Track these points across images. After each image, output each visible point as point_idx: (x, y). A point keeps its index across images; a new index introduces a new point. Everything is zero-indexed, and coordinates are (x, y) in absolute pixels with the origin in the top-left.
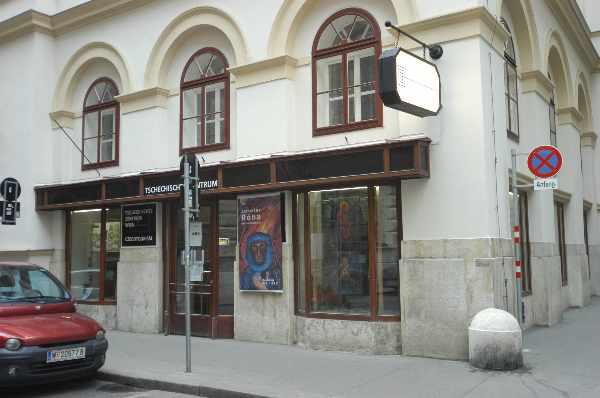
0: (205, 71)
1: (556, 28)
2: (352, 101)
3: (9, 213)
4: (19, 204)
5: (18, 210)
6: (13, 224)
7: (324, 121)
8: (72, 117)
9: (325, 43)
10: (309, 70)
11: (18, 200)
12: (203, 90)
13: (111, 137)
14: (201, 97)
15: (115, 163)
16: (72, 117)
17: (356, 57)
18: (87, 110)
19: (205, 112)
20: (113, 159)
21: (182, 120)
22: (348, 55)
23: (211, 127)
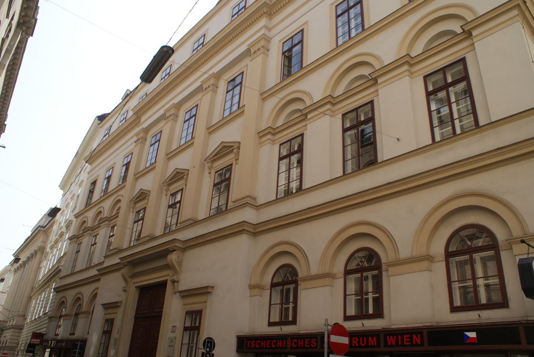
0: (284, 277)
1: (475, 265)
2: (367, 300)
7: (275, 318)
8: (429, 258)
9: (353, 266)
10: (269, 291)
11: (213, 352)
12: (283, 288)
13: (284, 307)
14: (282, 291)
15: (294, 322)
16: (429, 258)
17: (370, 274)
18: (273, 285)
19: (285, 300)
20: (197, 325)
21: (270, 305)
22: (364, 273)
23: (287, 309)
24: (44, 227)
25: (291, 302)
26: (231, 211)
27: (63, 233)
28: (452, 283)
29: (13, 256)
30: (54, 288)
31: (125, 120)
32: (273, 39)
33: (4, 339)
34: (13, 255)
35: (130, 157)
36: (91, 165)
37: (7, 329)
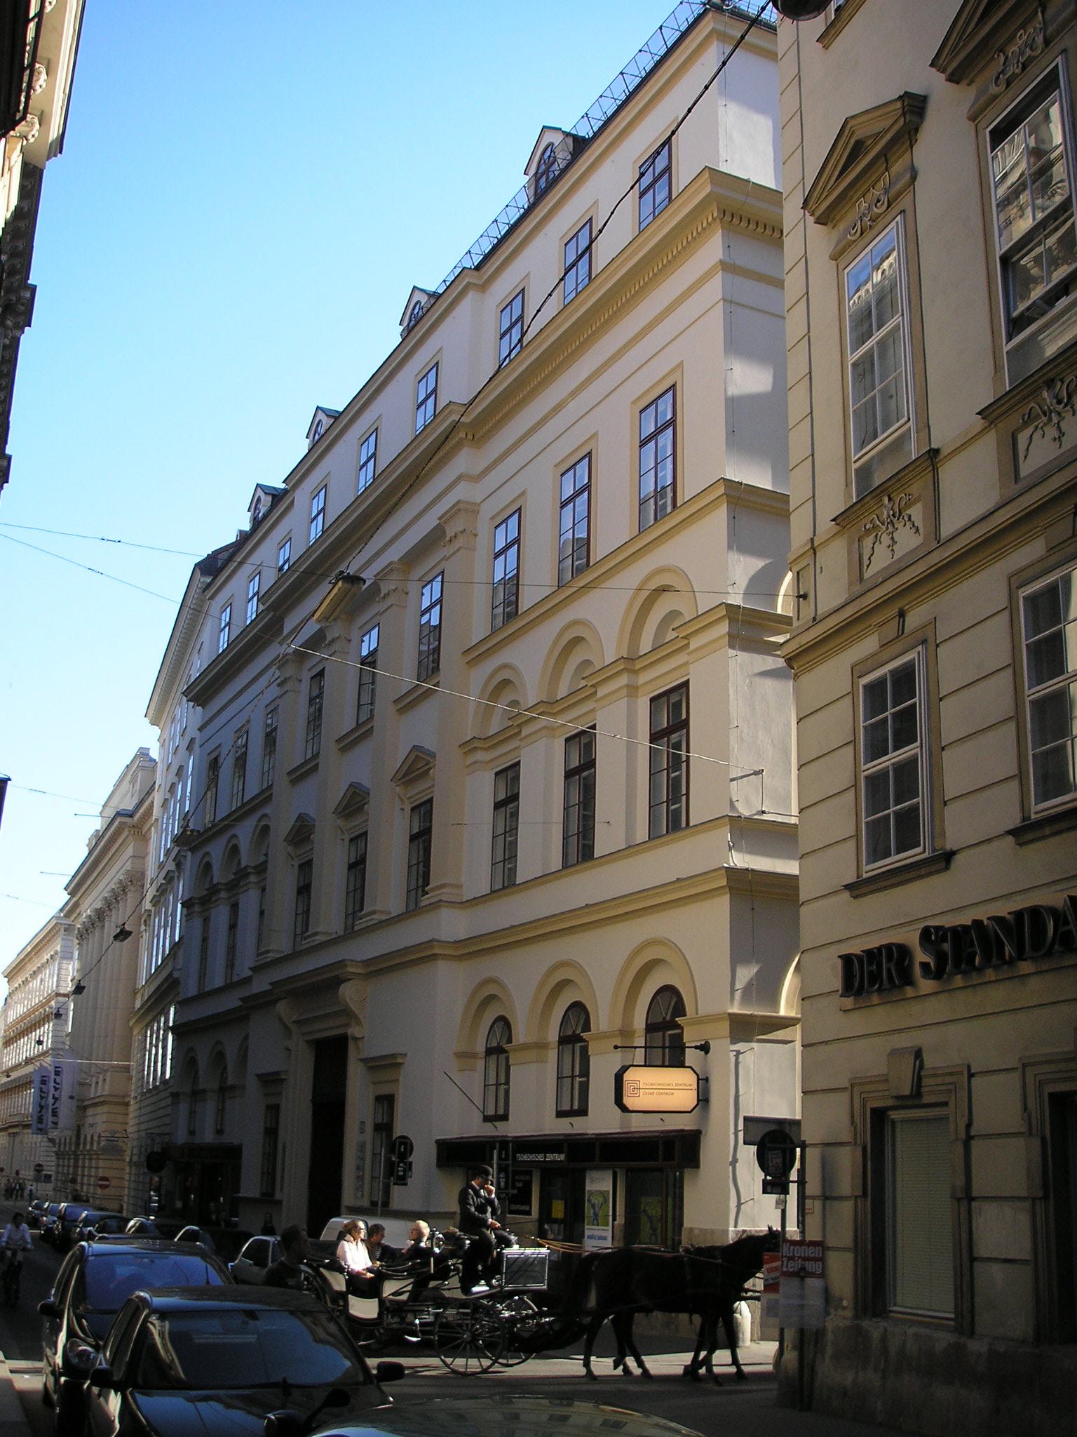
3: (401, 1173)
4: (411, 1163)
5: (410, 1169)
6: (406, 1184)
24: (131, 816)
25: (587, 1364)
26: (502, 418)
27: (171, 874)
28: (790, 1184)
29: (66, 893)
30: (173, 1029)
31: (256, 597)
32: (484, 506)
33: (91, 1131)
34: (65, 889)
35: (437, 585)
36: (203, 708)
37: (95, 1105)
